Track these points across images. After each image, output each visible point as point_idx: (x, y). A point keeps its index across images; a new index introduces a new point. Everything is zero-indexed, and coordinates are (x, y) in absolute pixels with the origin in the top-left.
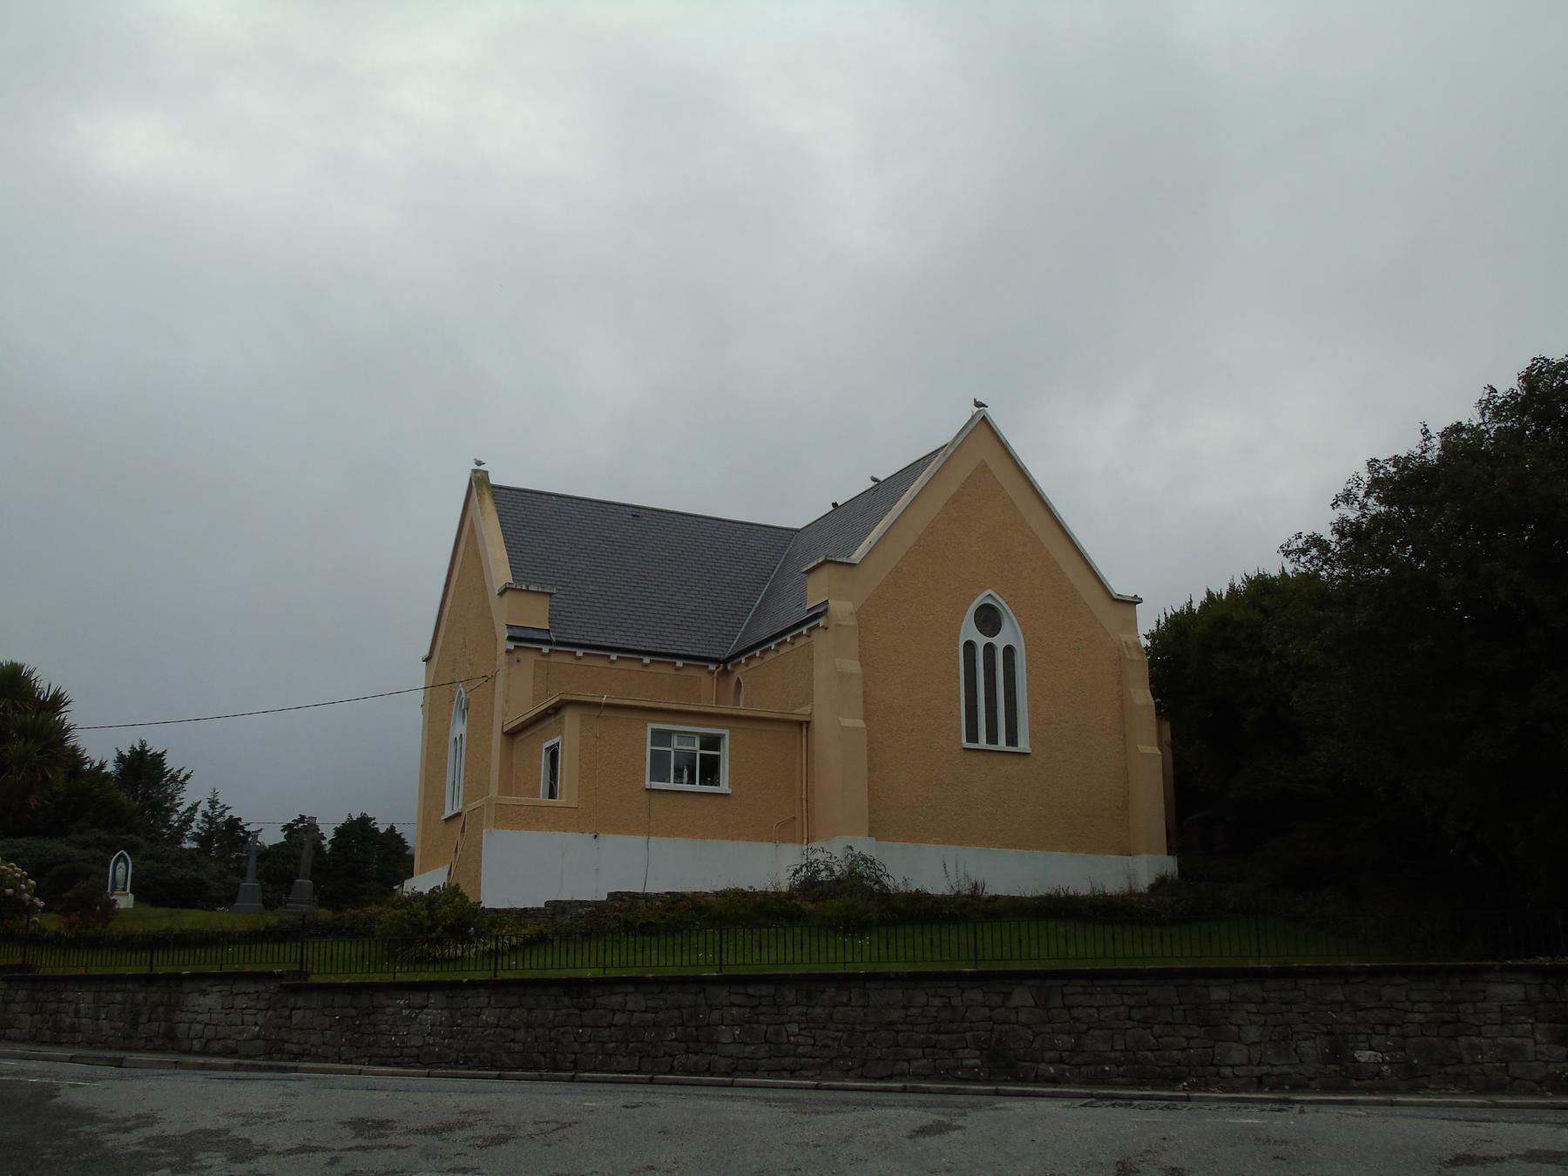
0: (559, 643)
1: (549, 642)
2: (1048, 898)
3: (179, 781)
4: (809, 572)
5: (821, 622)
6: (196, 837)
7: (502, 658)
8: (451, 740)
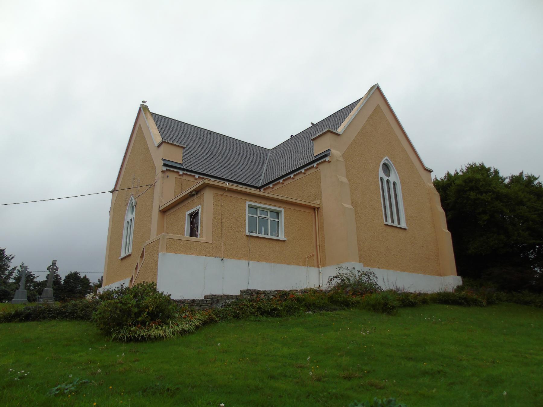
0: (188, 171)
1: (183, 169)
2: (439, 294)
3: (10, 259)
4: (313, 140)
5: (327, 159)
6: (15, 278)
7: (161, 174)
8: (126, 222)
